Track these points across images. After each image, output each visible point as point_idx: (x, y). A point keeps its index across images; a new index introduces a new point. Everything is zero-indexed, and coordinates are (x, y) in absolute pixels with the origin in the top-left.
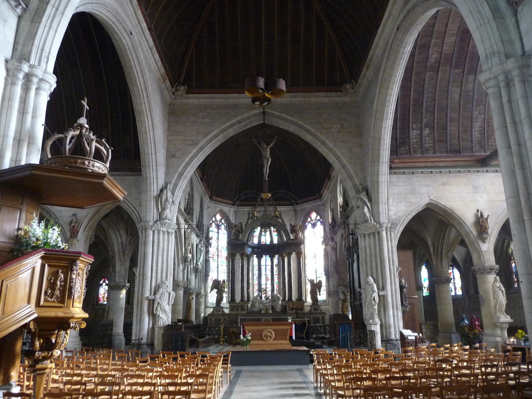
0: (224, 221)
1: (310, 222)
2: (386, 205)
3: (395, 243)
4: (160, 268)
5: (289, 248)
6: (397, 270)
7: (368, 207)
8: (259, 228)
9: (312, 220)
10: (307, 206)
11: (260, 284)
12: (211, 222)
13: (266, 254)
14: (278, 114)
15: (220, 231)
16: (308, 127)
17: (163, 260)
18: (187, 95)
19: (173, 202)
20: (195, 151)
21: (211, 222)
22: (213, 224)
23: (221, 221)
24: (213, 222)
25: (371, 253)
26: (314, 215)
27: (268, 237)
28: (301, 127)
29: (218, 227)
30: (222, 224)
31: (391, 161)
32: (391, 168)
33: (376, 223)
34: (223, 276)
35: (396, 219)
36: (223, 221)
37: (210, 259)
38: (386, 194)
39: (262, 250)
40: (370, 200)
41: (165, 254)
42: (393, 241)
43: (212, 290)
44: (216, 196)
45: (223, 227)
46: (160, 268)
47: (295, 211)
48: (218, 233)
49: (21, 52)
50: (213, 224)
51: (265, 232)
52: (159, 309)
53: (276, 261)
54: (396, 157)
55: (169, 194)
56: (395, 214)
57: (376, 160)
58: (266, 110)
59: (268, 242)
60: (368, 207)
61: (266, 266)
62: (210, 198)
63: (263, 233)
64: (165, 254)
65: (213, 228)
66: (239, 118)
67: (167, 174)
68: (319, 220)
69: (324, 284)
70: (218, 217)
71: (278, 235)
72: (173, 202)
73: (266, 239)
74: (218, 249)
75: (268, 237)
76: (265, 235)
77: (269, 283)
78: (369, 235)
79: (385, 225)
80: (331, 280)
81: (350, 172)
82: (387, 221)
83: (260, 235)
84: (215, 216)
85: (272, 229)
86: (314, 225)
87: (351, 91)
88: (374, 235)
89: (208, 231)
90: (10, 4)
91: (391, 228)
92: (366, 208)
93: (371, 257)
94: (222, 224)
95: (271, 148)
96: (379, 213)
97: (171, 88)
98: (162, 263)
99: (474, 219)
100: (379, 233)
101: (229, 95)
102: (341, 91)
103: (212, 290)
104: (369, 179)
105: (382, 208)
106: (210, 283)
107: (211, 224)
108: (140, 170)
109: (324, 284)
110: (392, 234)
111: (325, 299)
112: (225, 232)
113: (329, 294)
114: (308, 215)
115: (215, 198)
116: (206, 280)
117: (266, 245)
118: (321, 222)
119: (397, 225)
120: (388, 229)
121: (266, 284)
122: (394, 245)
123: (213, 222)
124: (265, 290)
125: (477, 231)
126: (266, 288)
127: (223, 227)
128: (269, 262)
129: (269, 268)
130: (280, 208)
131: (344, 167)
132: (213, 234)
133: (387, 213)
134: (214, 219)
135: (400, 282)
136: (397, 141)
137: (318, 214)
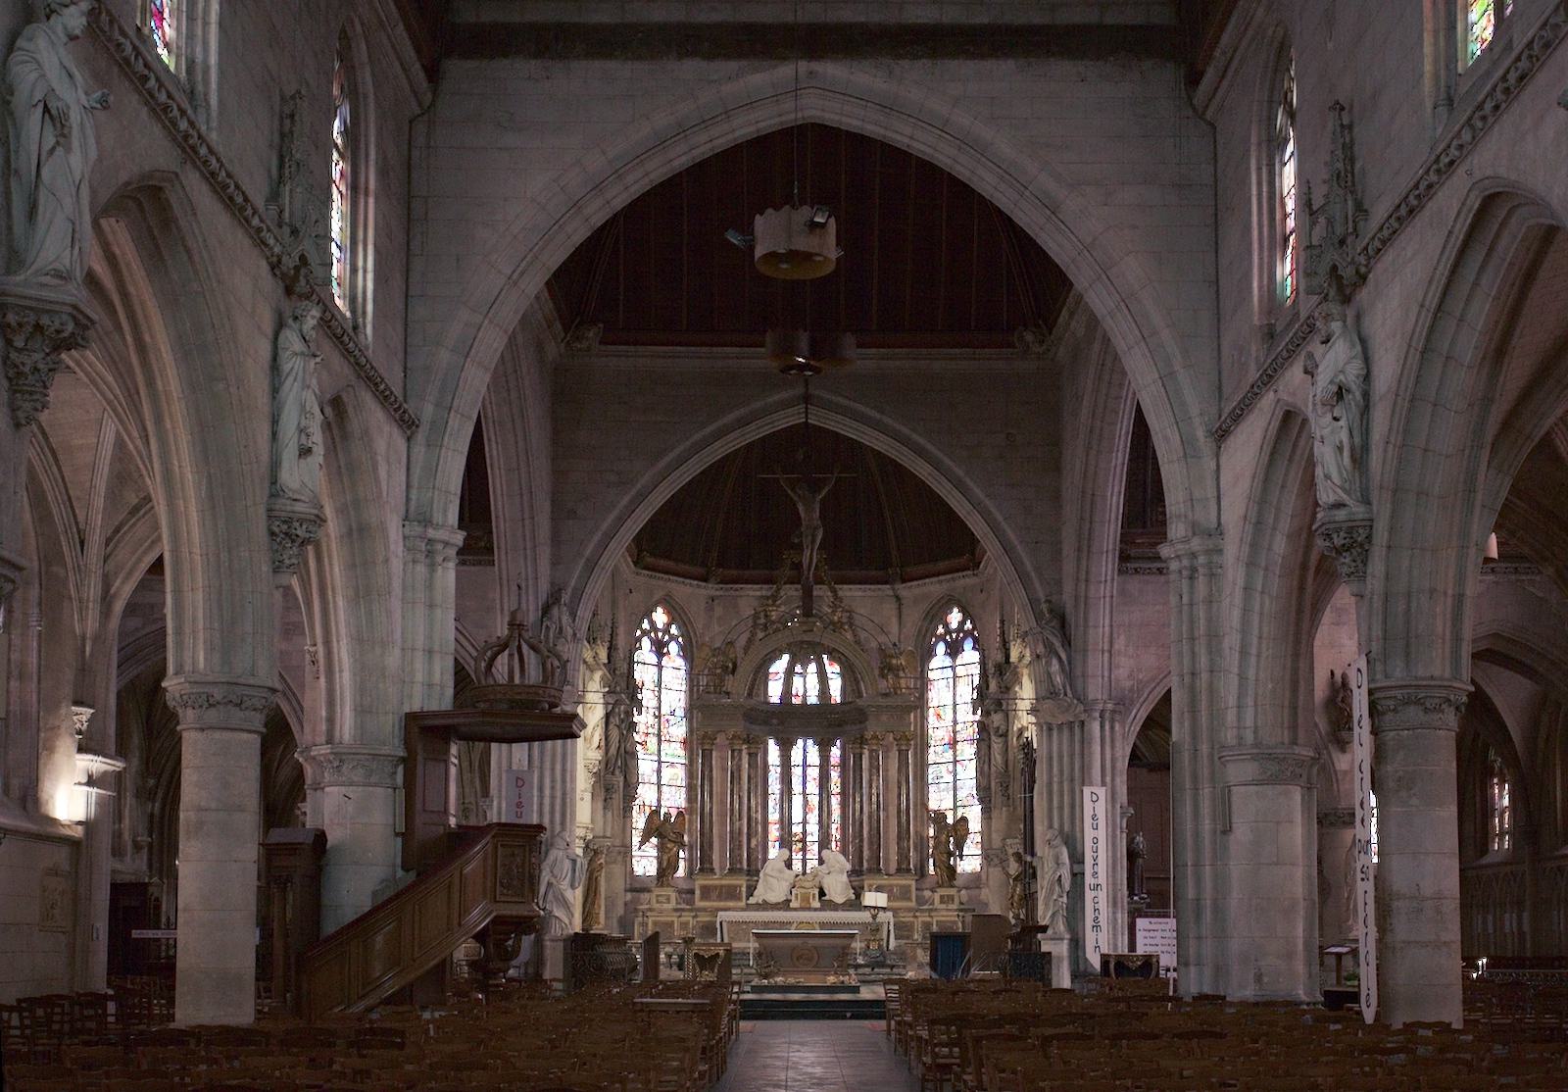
0: (679, 628)
1: (942, 638)
2: (1106, 655)
3: (1124, 752)
4: (547, 801)
5: (874, 725)
6: (1123, 814)
7: (1060, 659)
8: (786, 657)
9: (948, 631)
10: (934, 587)
11: (786, 823)
12: (639, 633)
13: (806, 736)
14: (846, 402)
15: (665, 661)
16: (921, 441)
17: (553, 781)
18: (603, 348)
19: (575, 635)
20: (625, 500)
21: (639, 633)
22: (646, 643)
23: (666, 631)
24: (645, 633)
25: (1061, 772)
26: (955, 618)
27: (810, 683)
28: (905, 441)
29: (660, 649)
30: (673, 638)
31: (1126, 539)
32: (1124, 558)
33: (1078, 699)
34: (675, 799)
35: (1131, 690)
36: (674, 630)
37: (639, 747)
38: (1107, 629)
39: (790, 721)
40: (1067, 642)
41: (558, 767)
42: (1118, 744)
43: (644, 840)
44: (653, 555)
45: (673, 647)
46: (547, 801)
47: (898, 598)
48: (660, 667)
49: (418, 499)
50: (646, 643)
51: (805, 666)
52: (550, 896)
53: (835, 752)
54: (1140, 531)
55: (566, 619)
56: (1130, 676)
57: (1085, 546)
58: (811, 390)
59: (813, 699)
60: (1060, 659)
61: (805, 765)
62: (636, 563)
63: (798, 668)
64: (558, 767)
65: (645, 653)
66: (742, 411)
67: (555, 563)
68: (969, 634)
69: (975, 824)
70: (660, 617)
71: (842, 675)
72: (575, 635)
73: (807, 687)
74: (659, 717)
75: (810, 683)
76: (803, 675)
77: (813, 818)
78: (1060, 727)
79: (1100, 706)
80: (995, 814)
81: (1022, 563)
82: (1105, 697)
83: (790, 673)
84: (648, 614)
85: (810, 742)
86: (954, 650)
87: (1037, 349)
88: (1071, 729)
89: (631, 663)
90: (349, 362)
91: (1113, 712)
92: (1055, 662)
93: (1061, 783)
94: (673, 638)
95: (823, 502)
96: (1084, 675)
97: (563, 335)
98: (553, 788)
99: (1327, 693)
100: (1082, 723)
101: (715, 349)
102: (1010, 345)
103: (644, 840)
104: (1068, 588)
105: (1096, 663)
106: (639, 821)
107: (639, 640)
108: (490, 550)
109: (975, 824)
110: (1117, 726)
111: (978, 869)
112: (680, 662)
113: (987, 856)
114: (938, 614)
115: (649, 560)
116: (627, 811)
117: (804, 704)
118: (976, 641)
119: (1132, 703)
120: (1107, 715)
121: (804, 822)
122: (1119, 754)
123: (645, 633)
124: (803, 841)
125: (1331, 722)
126: (804, 832)
127: (673, 647)
128: (814, 756)
129: (814, 773)
130: (848, 592)
131: (1008, 549)
132: (644, 674)
133: (1106, 674)
134: (646, 625)
135: (1131, 842)
136: (1145, 491)
137: (967, 614)
